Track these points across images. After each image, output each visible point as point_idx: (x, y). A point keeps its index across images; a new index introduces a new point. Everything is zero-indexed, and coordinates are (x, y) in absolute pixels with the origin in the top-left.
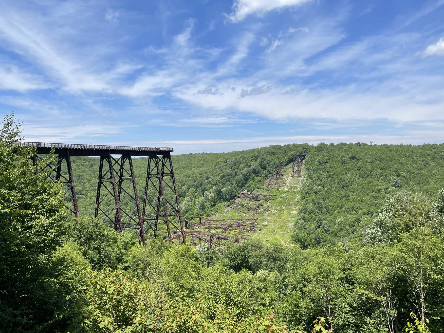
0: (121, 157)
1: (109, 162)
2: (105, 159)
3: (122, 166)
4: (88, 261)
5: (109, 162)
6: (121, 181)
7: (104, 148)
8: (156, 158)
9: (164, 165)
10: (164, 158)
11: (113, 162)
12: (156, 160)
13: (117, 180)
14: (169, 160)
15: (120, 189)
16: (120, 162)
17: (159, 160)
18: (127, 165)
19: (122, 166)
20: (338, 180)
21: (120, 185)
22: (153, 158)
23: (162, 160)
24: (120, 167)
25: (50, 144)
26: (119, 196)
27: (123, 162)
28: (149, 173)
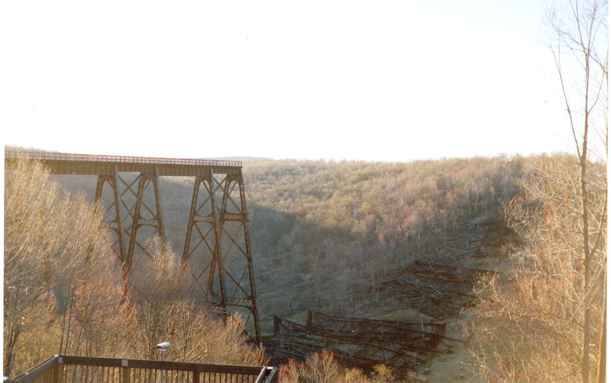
0: (226, 178)
1: (114, 186)
2: (106, 182)
3: (139, 196)
4: (372, 190)
5: (114, 186)
6: (136, 226)
7: (203, 163)
10: (229, 179)
11: (121, 186)
12: (210, 186)
14: (240, 185)
15: (132, 242)
16: (135, 188)
18: (149, 194)
19: (139, 196)
20: (365, 300)
21: (133, 235)
22: (205, 181)
24: (135, 200)
25: (225, 162)
26: (130, 256)
27: (141, 187)
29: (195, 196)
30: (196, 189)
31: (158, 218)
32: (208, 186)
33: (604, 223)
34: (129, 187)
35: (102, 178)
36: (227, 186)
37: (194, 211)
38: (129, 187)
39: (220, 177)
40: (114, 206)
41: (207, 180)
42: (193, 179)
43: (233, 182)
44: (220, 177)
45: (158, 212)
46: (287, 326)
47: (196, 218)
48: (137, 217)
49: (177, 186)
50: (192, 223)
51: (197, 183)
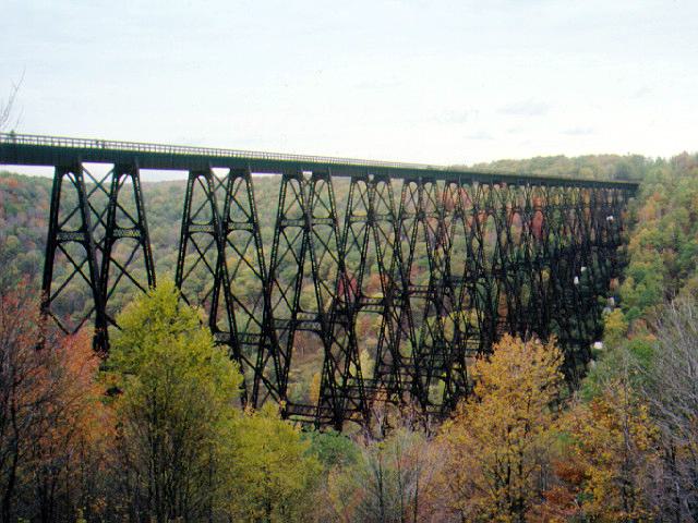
6: (110, 239)
8: (209, 175)
9: (230, 197)
13: (99, 233)
17: (217, 183)
18: (70, 196)
22: (71, 174)
23: (225, 183)
24: (107, 199)
28: (55, 227)
29: (189, 199)
30: (190, 190)
31: (140, 226)
32: (206, 185)
33: (313, 425)
34: (221, 183)
35: (287, 178)
36: (230, 185)
37: (189, 220)
38: (99, 185)
39: (221, 173)
40: (79, 213)
41: (73, 172)
42: (184, 175)
43: (239, 179)
44: (221, 173)
45: (141, 218)
46: (414, 345)
47: (283, 223)
48: (111, 227)
49: (36, 181)
50: (186, 234)
51: (58, 180)
